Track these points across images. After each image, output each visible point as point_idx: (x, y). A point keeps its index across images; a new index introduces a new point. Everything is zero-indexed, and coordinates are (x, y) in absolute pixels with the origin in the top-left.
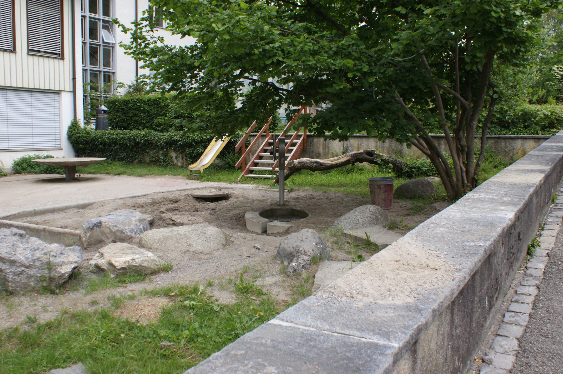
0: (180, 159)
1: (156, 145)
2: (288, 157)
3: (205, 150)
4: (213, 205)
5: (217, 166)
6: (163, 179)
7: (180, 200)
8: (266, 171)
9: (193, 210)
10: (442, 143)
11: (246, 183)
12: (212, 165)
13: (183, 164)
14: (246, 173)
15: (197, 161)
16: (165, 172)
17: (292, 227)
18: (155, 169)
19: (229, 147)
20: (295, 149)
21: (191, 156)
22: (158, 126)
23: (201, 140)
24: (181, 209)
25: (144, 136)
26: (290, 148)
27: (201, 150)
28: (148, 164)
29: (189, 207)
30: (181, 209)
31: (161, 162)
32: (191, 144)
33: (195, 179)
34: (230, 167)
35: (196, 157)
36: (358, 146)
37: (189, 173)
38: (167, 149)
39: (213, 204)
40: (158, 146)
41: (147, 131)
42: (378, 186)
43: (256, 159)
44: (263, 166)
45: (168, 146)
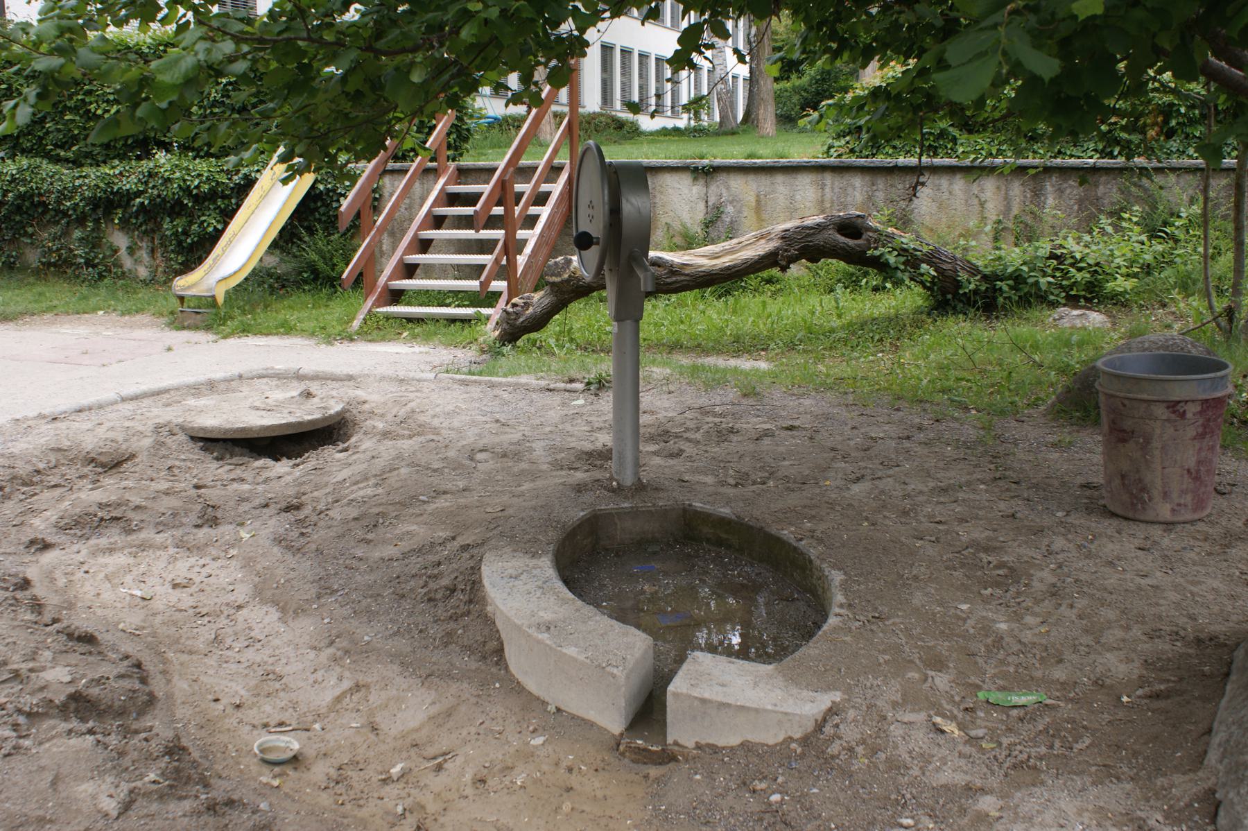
0: (144, 254)
1: (57, 211)
2: (525, 241)
3: (226, 225)
4: (282, 473)
5: (270, 275)
6: (83, 330)
7: (132, 456)
8: (456, 293)
9: (193, 518)
10: (1049, 187)
11: (383, 339)
12: (254, 273)
13: (154, 273)
14: (378, 303)
15: (200, 261)
16: (93, 301)
17: (833, 711)
18: (58, 292)
19: (311, 215)
20: (545, 212)
21: (180, 243)
22: (62, 147)
23: (213, 192)
24: (136, 517)
25: (13, 180)
26: (533, 210)
27: (212, 222)
28: (37, 273)
29: (173, 502)
30: (136, 517)
31: (79, 266)
32: (179, 202)
33: (196, 328)
34: (315, 280)
35: (196, 250)
36: (758, 201)
37: (175, 303)
38: (97, 221)
39: (283, 467)
40: (65, 214)
41: (25, 162)
42: (1173, 406)
43: (409, 250)
44: (428, 276)
45: (100, 212)
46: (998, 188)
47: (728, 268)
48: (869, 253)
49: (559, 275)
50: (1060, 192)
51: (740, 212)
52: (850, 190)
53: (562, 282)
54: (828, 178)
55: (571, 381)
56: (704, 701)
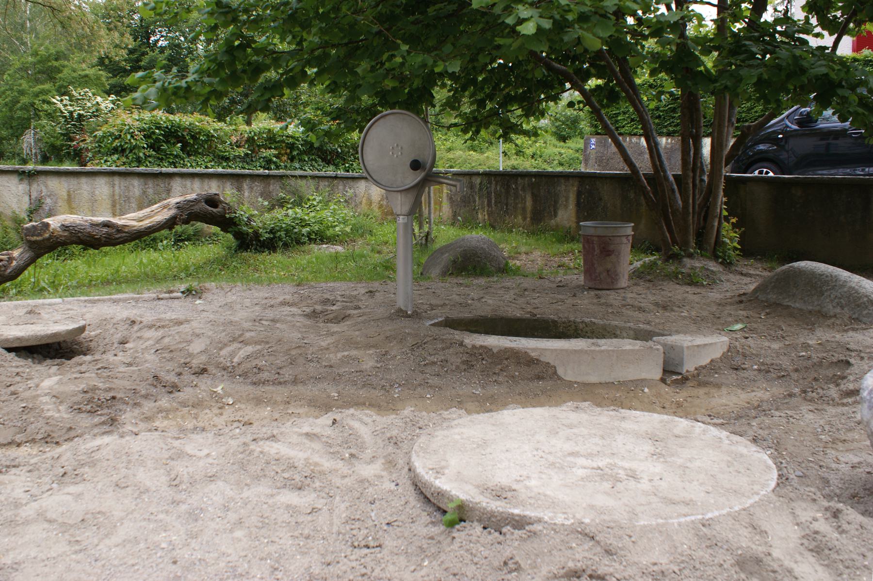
36: (69, 195)
46: (219, 186)
47: (149, 227)
48: (228, 216)
49: (40, 235)
50: (251, 188)
51: (56, 203)
52: (131, 187)
53: (43, 240)
54: (117, 180)
55: (171, 292)
56: (698, 346)
